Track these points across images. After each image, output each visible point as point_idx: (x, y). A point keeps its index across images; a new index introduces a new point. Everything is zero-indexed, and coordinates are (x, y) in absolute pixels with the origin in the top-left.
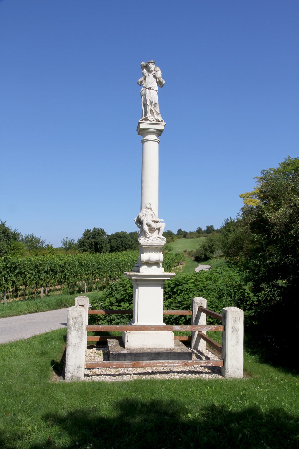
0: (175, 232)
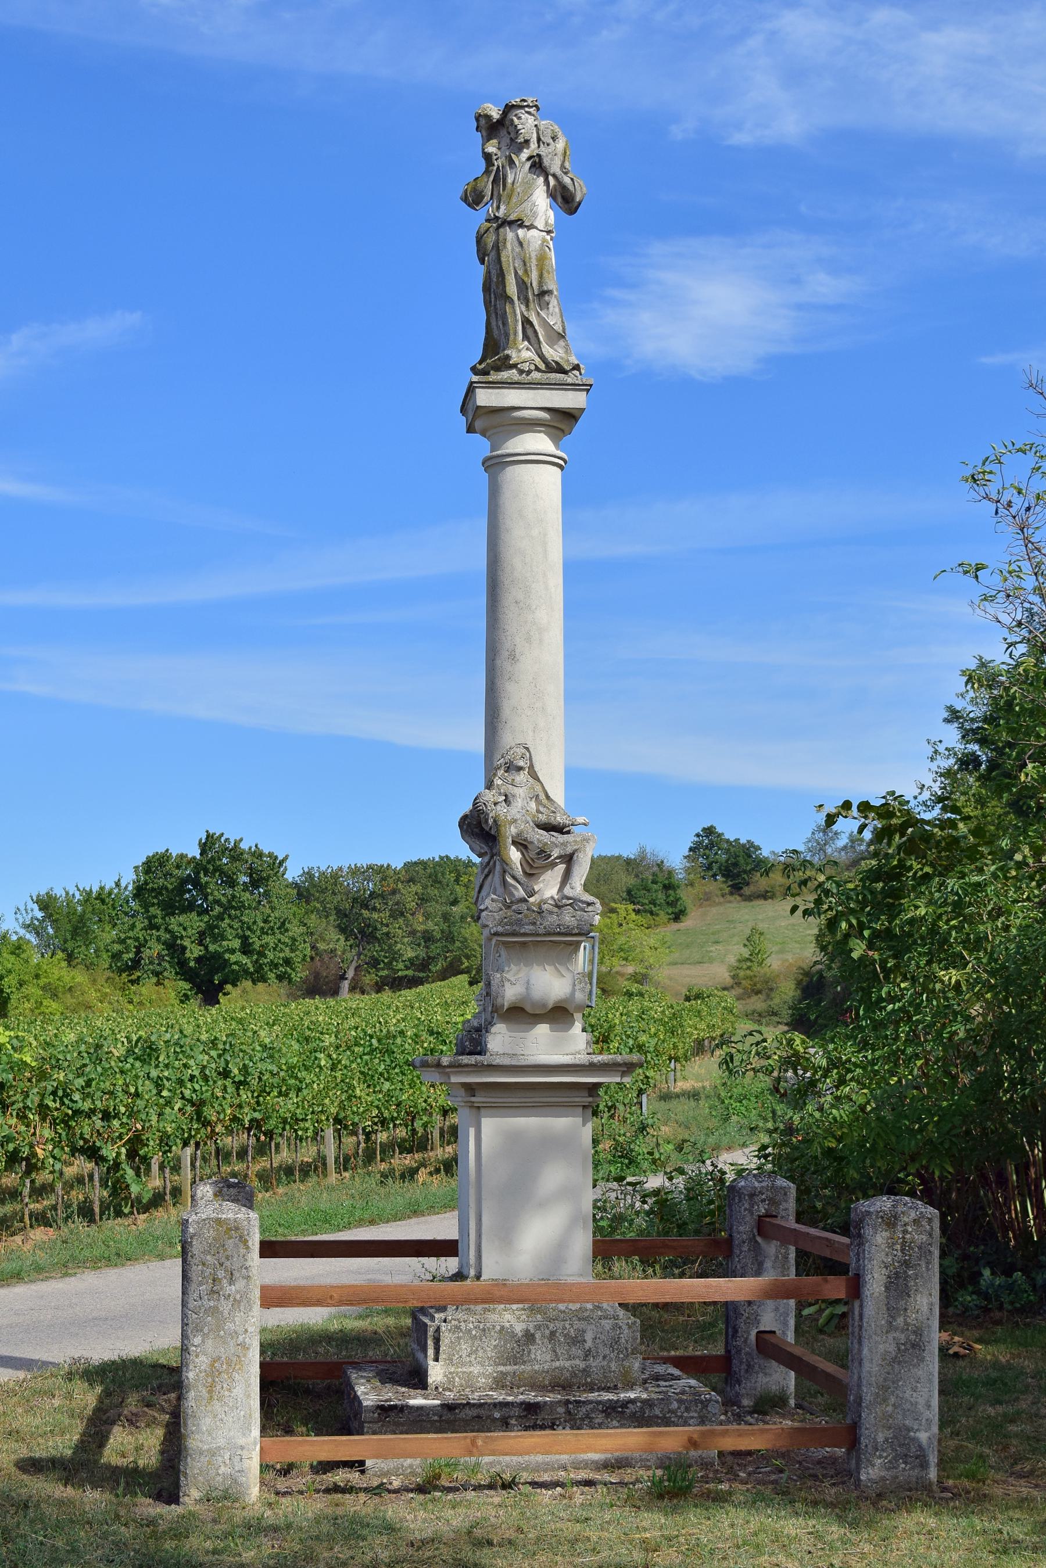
0: (674, 853)
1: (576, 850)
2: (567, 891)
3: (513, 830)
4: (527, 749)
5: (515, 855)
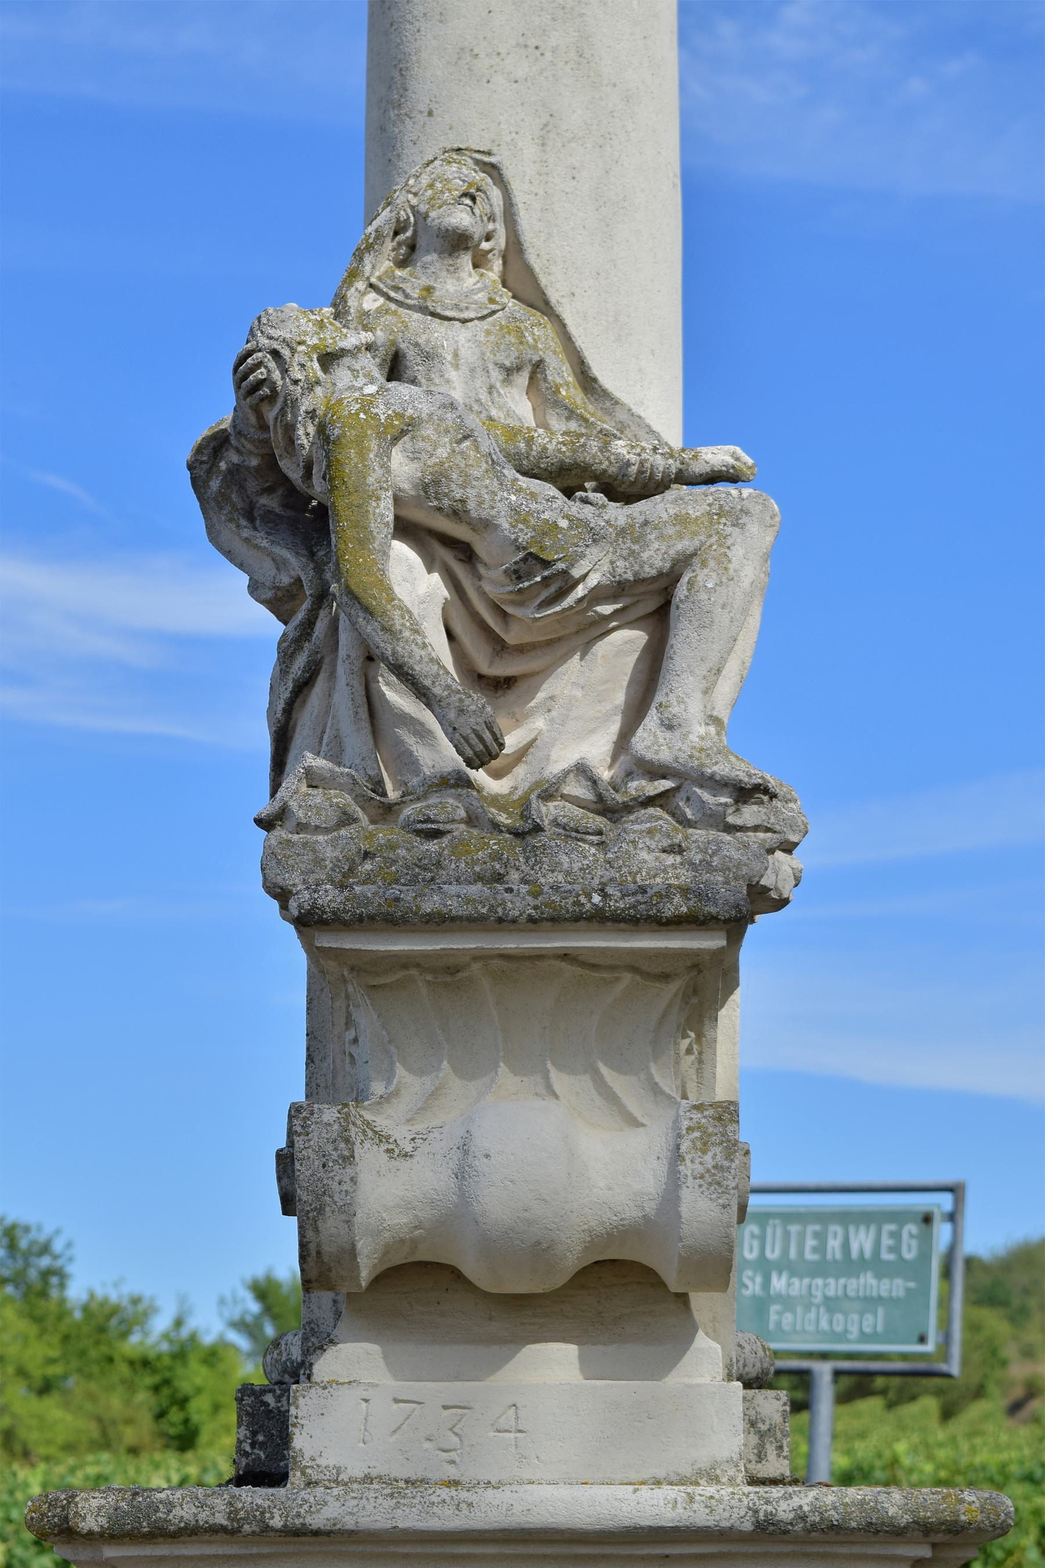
1: (682, 563)
2: (651, 740)
3: (402, 468)
4: (493, 170)
5: (413, 584)
